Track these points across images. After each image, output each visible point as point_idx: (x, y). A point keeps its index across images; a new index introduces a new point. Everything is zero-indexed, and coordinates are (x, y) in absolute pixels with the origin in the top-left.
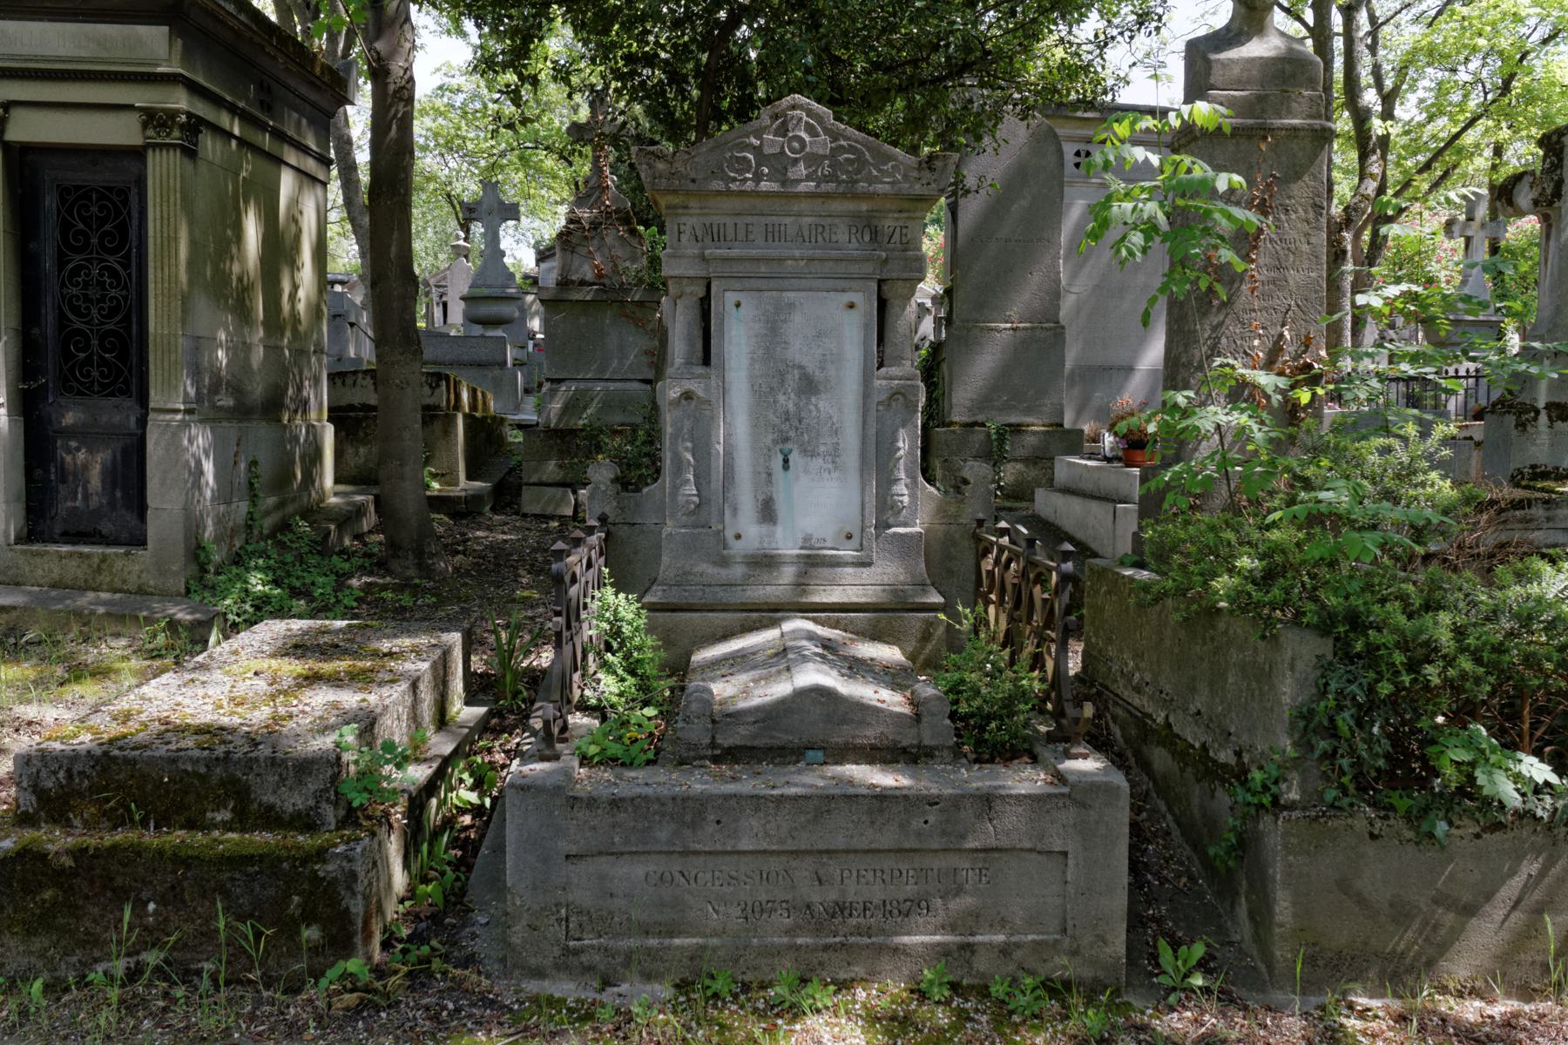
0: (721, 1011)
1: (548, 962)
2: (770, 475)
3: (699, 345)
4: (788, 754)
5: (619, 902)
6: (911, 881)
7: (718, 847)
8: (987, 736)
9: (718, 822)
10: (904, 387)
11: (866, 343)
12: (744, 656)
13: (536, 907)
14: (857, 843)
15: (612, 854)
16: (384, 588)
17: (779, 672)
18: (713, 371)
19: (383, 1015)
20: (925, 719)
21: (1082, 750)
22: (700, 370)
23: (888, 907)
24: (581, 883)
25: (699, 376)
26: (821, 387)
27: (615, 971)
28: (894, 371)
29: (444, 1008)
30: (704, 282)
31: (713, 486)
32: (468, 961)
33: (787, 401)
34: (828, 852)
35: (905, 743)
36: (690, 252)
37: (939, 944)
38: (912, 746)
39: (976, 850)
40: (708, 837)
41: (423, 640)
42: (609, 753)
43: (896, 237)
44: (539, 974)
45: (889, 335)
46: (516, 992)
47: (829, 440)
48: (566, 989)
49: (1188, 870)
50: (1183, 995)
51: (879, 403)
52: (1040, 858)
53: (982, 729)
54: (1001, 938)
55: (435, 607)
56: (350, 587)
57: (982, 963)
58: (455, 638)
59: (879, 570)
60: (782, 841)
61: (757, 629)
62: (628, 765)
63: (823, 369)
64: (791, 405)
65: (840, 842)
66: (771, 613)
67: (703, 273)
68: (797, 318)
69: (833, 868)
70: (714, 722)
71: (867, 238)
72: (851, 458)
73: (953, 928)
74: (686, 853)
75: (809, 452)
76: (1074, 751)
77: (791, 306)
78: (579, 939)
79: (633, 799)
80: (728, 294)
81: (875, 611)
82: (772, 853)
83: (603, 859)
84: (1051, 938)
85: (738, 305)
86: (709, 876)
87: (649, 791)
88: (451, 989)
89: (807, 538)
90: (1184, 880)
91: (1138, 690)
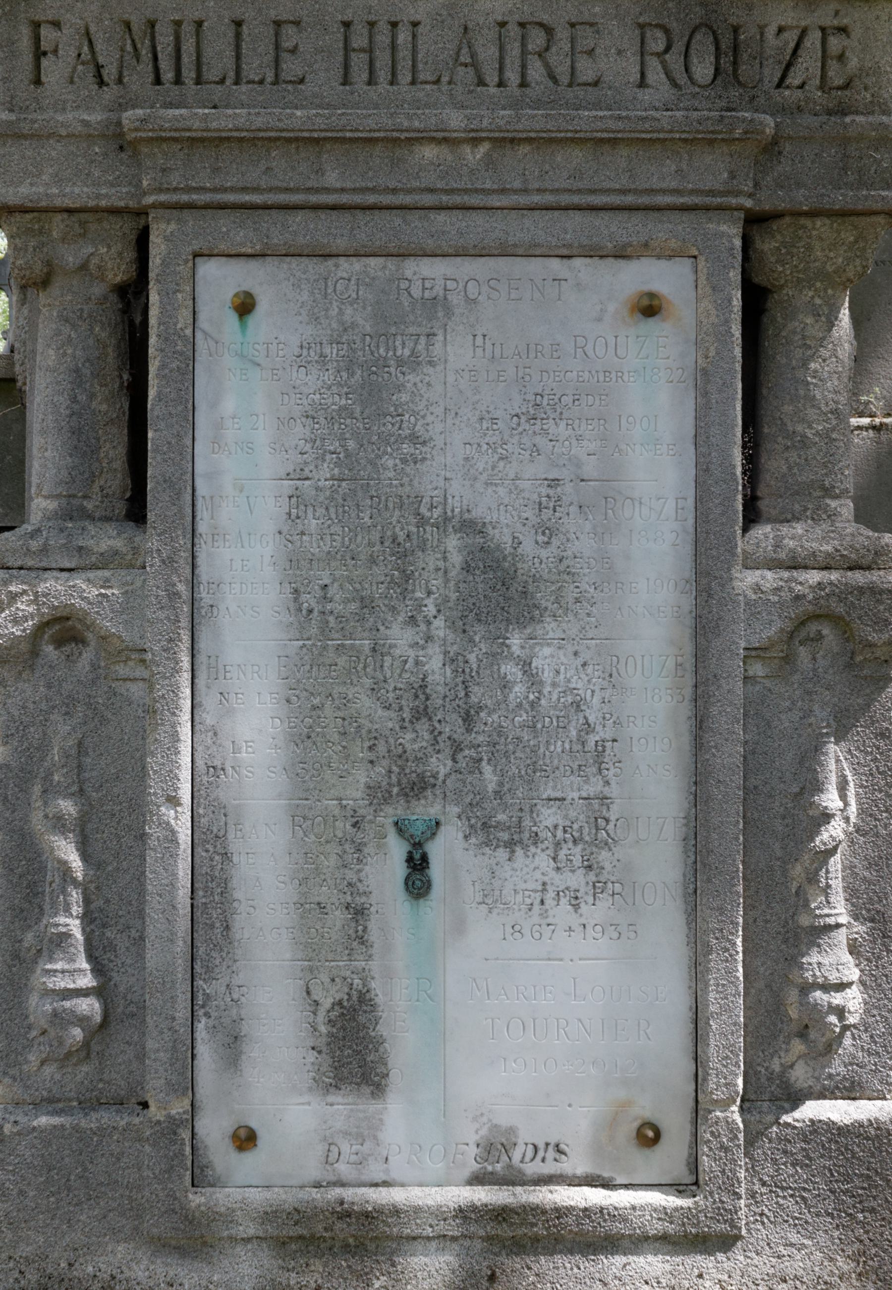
2: (359, 913)
3: (114, 451)
10: (843, 593)
11: (701, 438)
18: (152, 541)
22: (108, 539)
25: (106, 561)
26: (544, 597)
28: (798, 536)
30: (128, 227)
31: (153, 958)
33: (421, 649)
36: (70, 119)
43: (808, 65)
45: (778, 408)
47: (574, 788)
51: (753, 653)
59: (763, 1264)
63: (548, 532)
64: (434, 664)
67: (116, 196)
68: (457, 351)
71: (703, 70)
72: (655, 854)
75: (500, 831)
77: (436, 306)
80: (208, 269)
85: (245, 307)
89: (496, 1145)
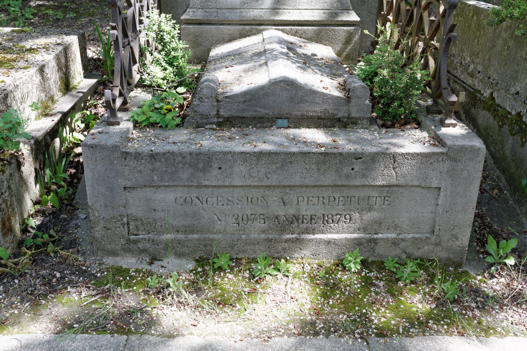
0: (223, 279)
1: (118, 247)
4: (265, 122)
5: (159, 214)
6: (341, 203)
7: (220, 183)
8: (390, 110)
9: (220, 168)
12: (240, 54)
13: (107, 217)
14: (307, 182)
15: (154, 187)
16: (48, 7)
17: (260, 66)
19: (16, 281)
20: (353, 101)
21: (454, 122)
23: (326, 218)
24: (136, 204)
27: (159, 252)
29: (54, 276)
32: (73, 244)
34: (289, 186)
35: (340, 115)
37: (355, 239)
38: (344, 117)
39: (383, 186)
40: (213, 177)
41: (53, 40)
42: (151, 120)
44: (113, 253)
46: (100, 264)
48: (129, 262)
49: (498, 185)
50: (499, 267)
52: (423, 191)
53: (388, 105)
54: (394, 235)
55: (75, 19)
56: (30, 7)
57: (380, 250)
58: (73, 40)
60: (260, 180)
61: (249, 36)
62: (165, 127)
65: (297, 180)
66: (255, 26)
69: (292, 196)
70: (218, 101)
73: (365, 230)
74: (200, 186)
76: (448, 121)
78: (136, 235)
79: (164, 154)
81: (318, 25)
82: (254, 187)
83: (148, 189)
84: (424, 236)
86: (215, 199)
87: (174, 148)
88: (60, 263)
90: (496, 191)
91: (472, 75)
